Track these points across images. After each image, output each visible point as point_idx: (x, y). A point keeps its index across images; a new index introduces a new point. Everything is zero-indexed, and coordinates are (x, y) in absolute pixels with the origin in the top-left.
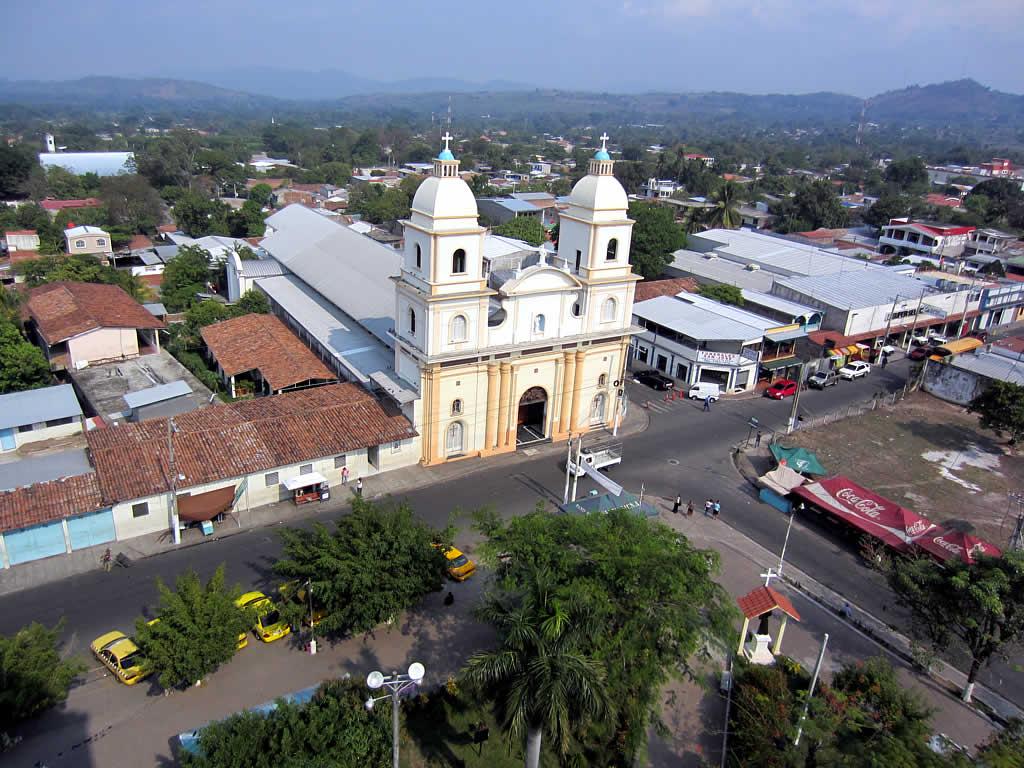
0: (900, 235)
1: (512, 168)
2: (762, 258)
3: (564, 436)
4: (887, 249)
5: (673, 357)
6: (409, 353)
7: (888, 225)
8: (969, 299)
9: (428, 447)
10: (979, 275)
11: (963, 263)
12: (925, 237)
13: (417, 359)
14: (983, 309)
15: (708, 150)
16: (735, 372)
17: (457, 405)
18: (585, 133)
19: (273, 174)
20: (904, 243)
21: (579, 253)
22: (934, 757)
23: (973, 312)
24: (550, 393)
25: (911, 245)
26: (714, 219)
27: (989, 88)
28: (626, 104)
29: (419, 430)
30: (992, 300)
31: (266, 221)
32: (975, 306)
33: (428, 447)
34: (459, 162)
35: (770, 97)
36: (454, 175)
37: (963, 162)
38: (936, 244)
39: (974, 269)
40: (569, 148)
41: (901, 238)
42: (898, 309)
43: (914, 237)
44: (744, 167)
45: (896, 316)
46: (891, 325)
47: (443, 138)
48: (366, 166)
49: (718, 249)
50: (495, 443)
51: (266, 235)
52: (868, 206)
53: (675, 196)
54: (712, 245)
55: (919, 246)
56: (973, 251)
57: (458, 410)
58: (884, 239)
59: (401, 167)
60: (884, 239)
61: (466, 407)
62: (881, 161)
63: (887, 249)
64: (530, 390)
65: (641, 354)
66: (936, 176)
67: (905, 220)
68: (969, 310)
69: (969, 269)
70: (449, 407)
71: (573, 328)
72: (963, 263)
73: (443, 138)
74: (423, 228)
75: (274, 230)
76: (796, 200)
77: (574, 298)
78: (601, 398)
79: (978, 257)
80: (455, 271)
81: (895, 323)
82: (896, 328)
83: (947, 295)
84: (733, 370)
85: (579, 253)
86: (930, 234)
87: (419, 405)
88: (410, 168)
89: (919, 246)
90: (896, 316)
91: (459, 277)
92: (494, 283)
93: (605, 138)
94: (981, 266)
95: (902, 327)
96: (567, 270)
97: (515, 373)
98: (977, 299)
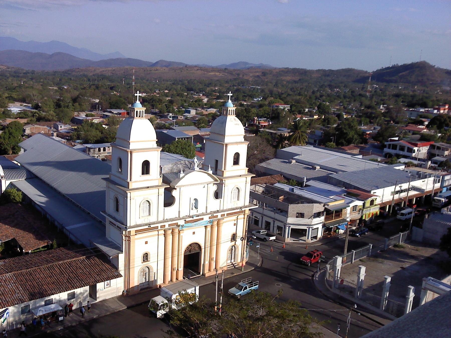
0: (394, 147)
1: (173, 112)
2: (321, 162)
3: (213, 273)
4: (388, 156)
5: (274, 222)
6: (115, 225)
7: (388, 142)
8: (435, 182)
9: (127, 281)
10: (439, 168)
11: (430, 162)
12: (408, 148)
13: (120, 228)
14: (442, 187)
15: (281, 97)
16: (311, 229)
17: (146, 257)
18: (215, 91)
19: (23, 115)
20: (397, 151)
21: (217, 161)
22: (67, 134)
23: (438, 189)
24: (203, 247)
25: (401, 153)
26: (293, 141)
27: (435, 66)
28: (238, 75)
29: (122, 273)
30: (447, 182)
31: (20, 144)
32: (438, 185)
33: (127, 281)
34: (145, 108)
35: (318, 71)
36: (142, 117)
37: (424, 105)
38: (414, 152)
39: (436, 165)
40: (205, 100)
41: (396, 149)
42: (398, 189)
43: (402, 149)
44: (307, 110)
45: (397, 192)
46: (395, 198)
47: (136, 95)
48: (83, 111)
49: (295, 157)
50: (170, 279)
51: (20, 153)
52: (376, 131)
53: (270, 127)
54: (292, 156)
55: (405, 153)
56: (434, 155)
57: (147, 259)
58: (386, 150)
59: (104, 112)
60: (386, 150)
61: (152, 258)
62: (382, 106)
63: (388, 156)
64: (190, 245)
65: (255, 220)
66: (411, 114)
67: (397, 139)
68: (435, 188)
69: (433, 165)
70: (141, 259)
71: (214, 205)
72: (430, 162)
73: (136, 95)
74: (328, 330)
75: (25, 151)
76: (337, 129)
77: (215, 188)
78: (233, 249)
79: (437, 158)
80: (143, 174)
81: (397, 197)
82: (397, 200)
83: (423, 180)
84: (309, 228)
85: (217, 161)
86: (410, 146)
87: (122, 257)
88: (110, 112)
89: (405, 153)
90: (397, 192)
91: (146, 177)
92: (166, 180)
93: (230, 94)
94: (439, 163)
95: (400, 199)
96: (210, 172)
97: (181, 234)
98: (439, 182)
